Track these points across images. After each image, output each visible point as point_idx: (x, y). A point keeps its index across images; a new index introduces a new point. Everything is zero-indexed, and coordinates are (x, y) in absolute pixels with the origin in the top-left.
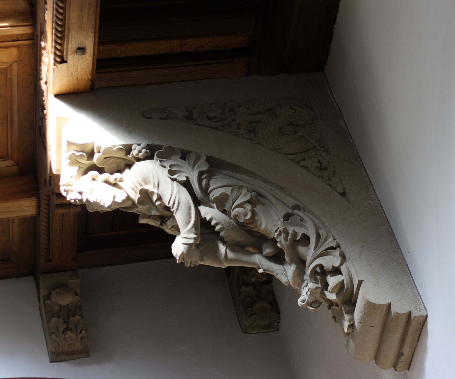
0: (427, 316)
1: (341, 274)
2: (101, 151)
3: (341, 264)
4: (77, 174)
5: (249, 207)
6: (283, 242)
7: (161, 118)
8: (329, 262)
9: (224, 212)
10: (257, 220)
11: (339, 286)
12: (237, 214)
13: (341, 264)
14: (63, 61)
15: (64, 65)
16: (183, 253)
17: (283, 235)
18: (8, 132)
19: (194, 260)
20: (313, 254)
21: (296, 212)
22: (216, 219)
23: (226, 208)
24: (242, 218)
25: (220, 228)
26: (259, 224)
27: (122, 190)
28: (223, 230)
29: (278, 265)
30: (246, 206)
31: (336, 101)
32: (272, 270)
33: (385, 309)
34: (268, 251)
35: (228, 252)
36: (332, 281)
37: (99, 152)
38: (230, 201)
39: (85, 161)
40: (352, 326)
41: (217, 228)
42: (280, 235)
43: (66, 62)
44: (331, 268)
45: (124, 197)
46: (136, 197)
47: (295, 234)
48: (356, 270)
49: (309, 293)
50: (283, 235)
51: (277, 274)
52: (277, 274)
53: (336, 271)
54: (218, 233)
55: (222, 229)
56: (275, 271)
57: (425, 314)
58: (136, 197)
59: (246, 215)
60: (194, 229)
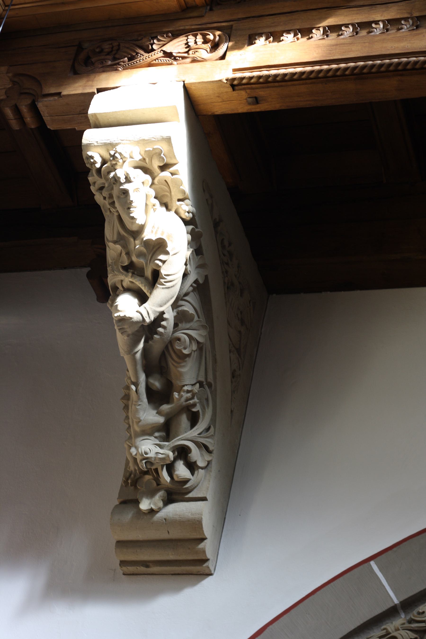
0: (211, 574)
1: (193, 474)
2: (174, 176)
3: (202, 468)
4: (136, 161)
5: (194, 347)
6: (183, 399)
7: (207, 200)
8: (196, 454)
9: (176, 325)
10: (186, 361)
11: (186, 480)
12: (182, 339)
13: (202, 468)
14: (233, 86)
15: (230, 89)
16: (131, 318)
17: (189, 395)
18: (49, 4)
19: (127, 330)
20: (195, 436)
21: (206, 387)
22: (168, 323)
23: (180, 325)
24: (181, 346)
25: (162, 332)
26: (182, 364)
27: (145, 216)
28: (160, 335)
29: (147, 400)
30: (193, 344)
31: (263, 330)
32: (141, 397)
33: (198, 536)
34: (157, 384)
35: (140, 352)
36: (182, 471)
37: (172, 174)
38: (188, 325)
39: (156, 164)
40: (152, 512)
41: (160, 330)
42: (188, 392)
43: (234, 90)
44: (193, 461)
45: (140, 221)
46: (148, 235)
47: (194, 405)
48: (205, 484)
49: (160, 456)
50: (189, 395)
51: (140, 405)
52: (140, 405)
53: (192, 467)
54: (156, 333)
55: (161, 334)
56: (142, 401)
57: (213, 572)
58: (148, 235)
59: (185, 348)
60: (158, 314)
